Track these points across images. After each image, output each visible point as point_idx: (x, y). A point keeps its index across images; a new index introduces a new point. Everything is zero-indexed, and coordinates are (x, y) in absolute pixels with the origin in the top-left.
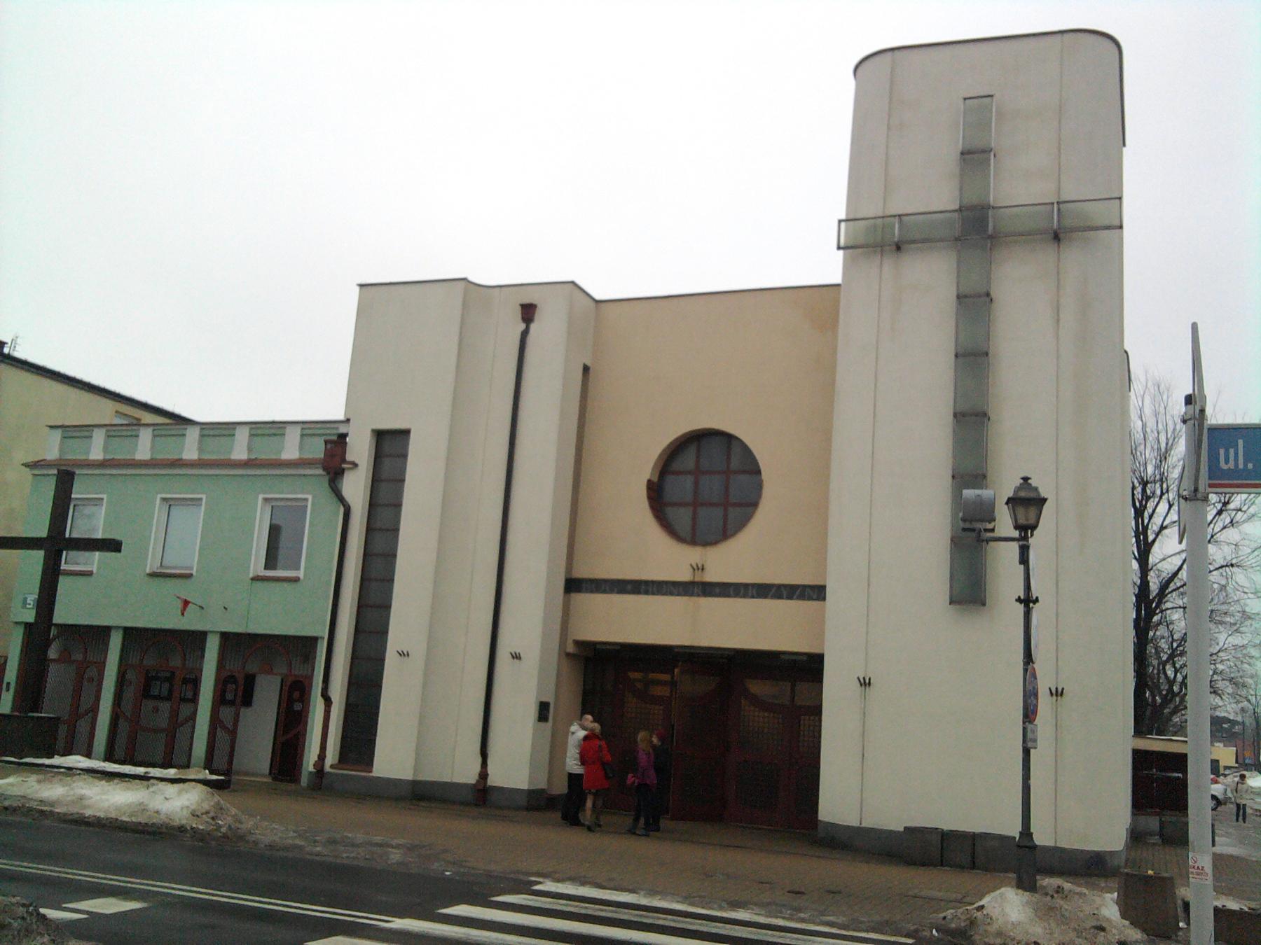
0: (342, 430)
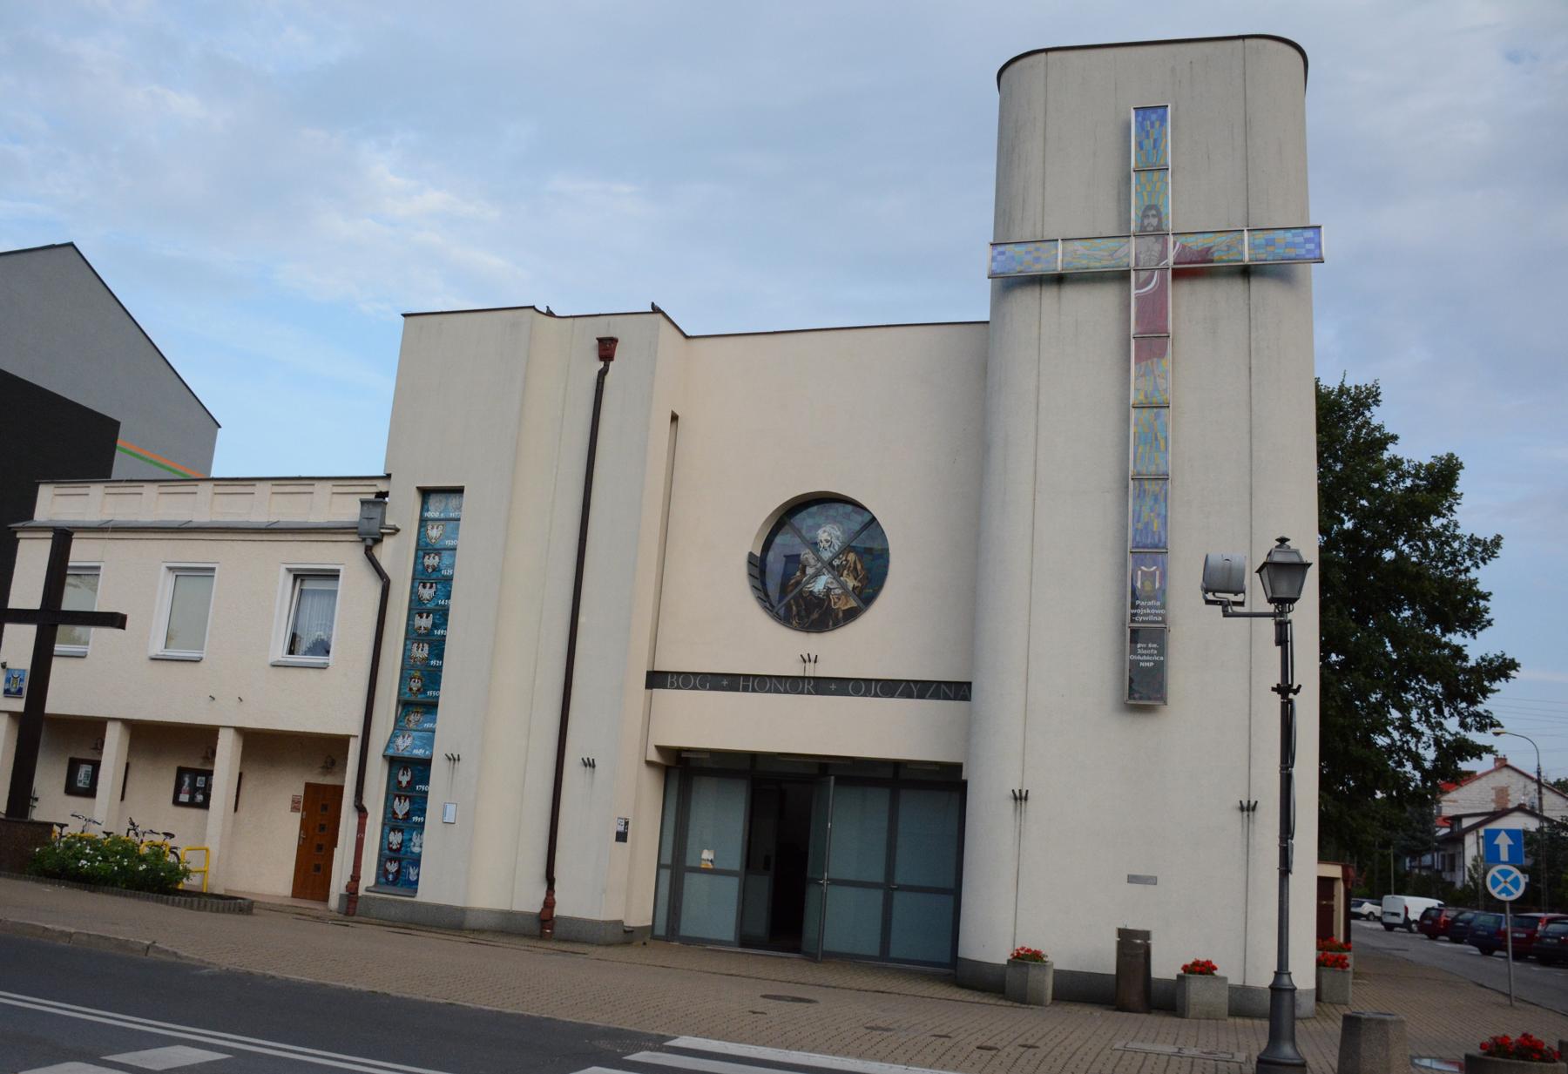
0: (382, 486)
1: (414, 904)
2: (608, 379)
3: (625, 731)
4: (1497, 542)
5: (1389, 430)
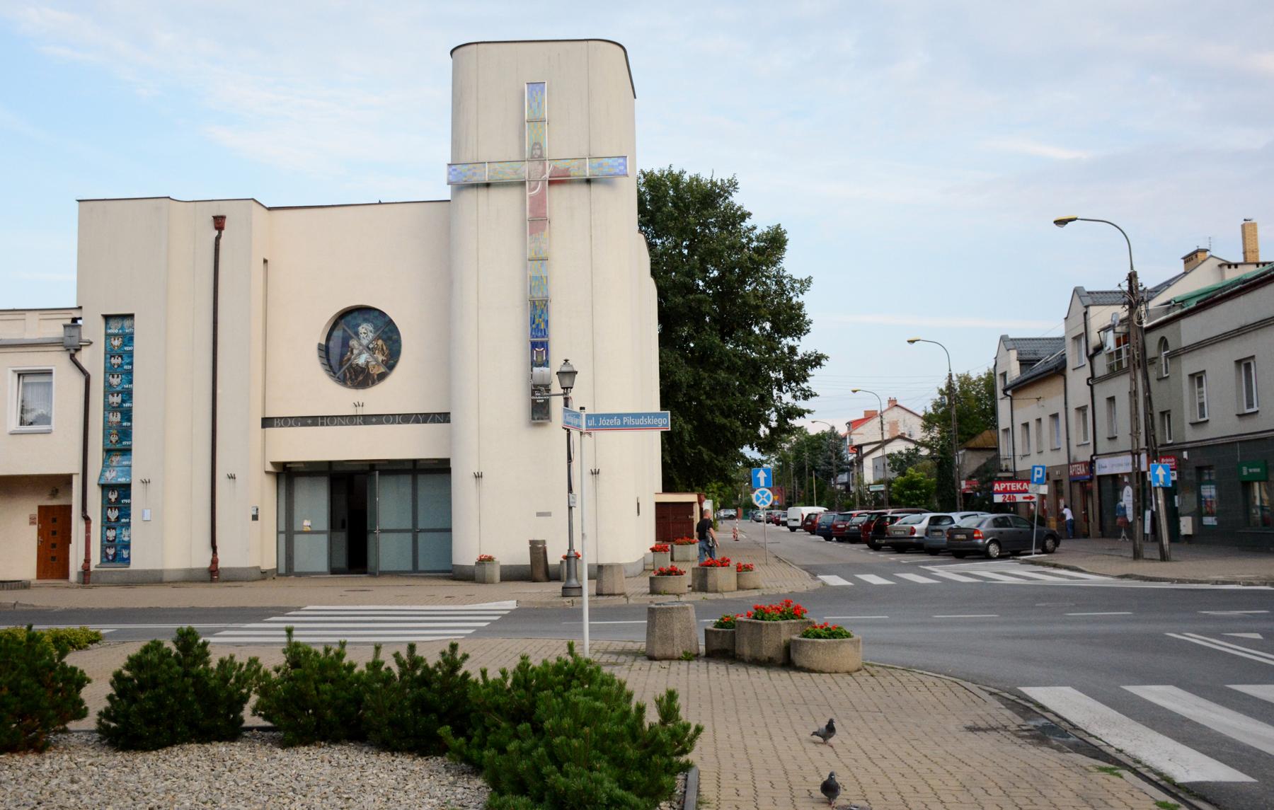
0: (76, 314)
1: (129, 572)
2: (222, 241)
3: (250, 457)
4: (809, 281)
5: (746, 209)
